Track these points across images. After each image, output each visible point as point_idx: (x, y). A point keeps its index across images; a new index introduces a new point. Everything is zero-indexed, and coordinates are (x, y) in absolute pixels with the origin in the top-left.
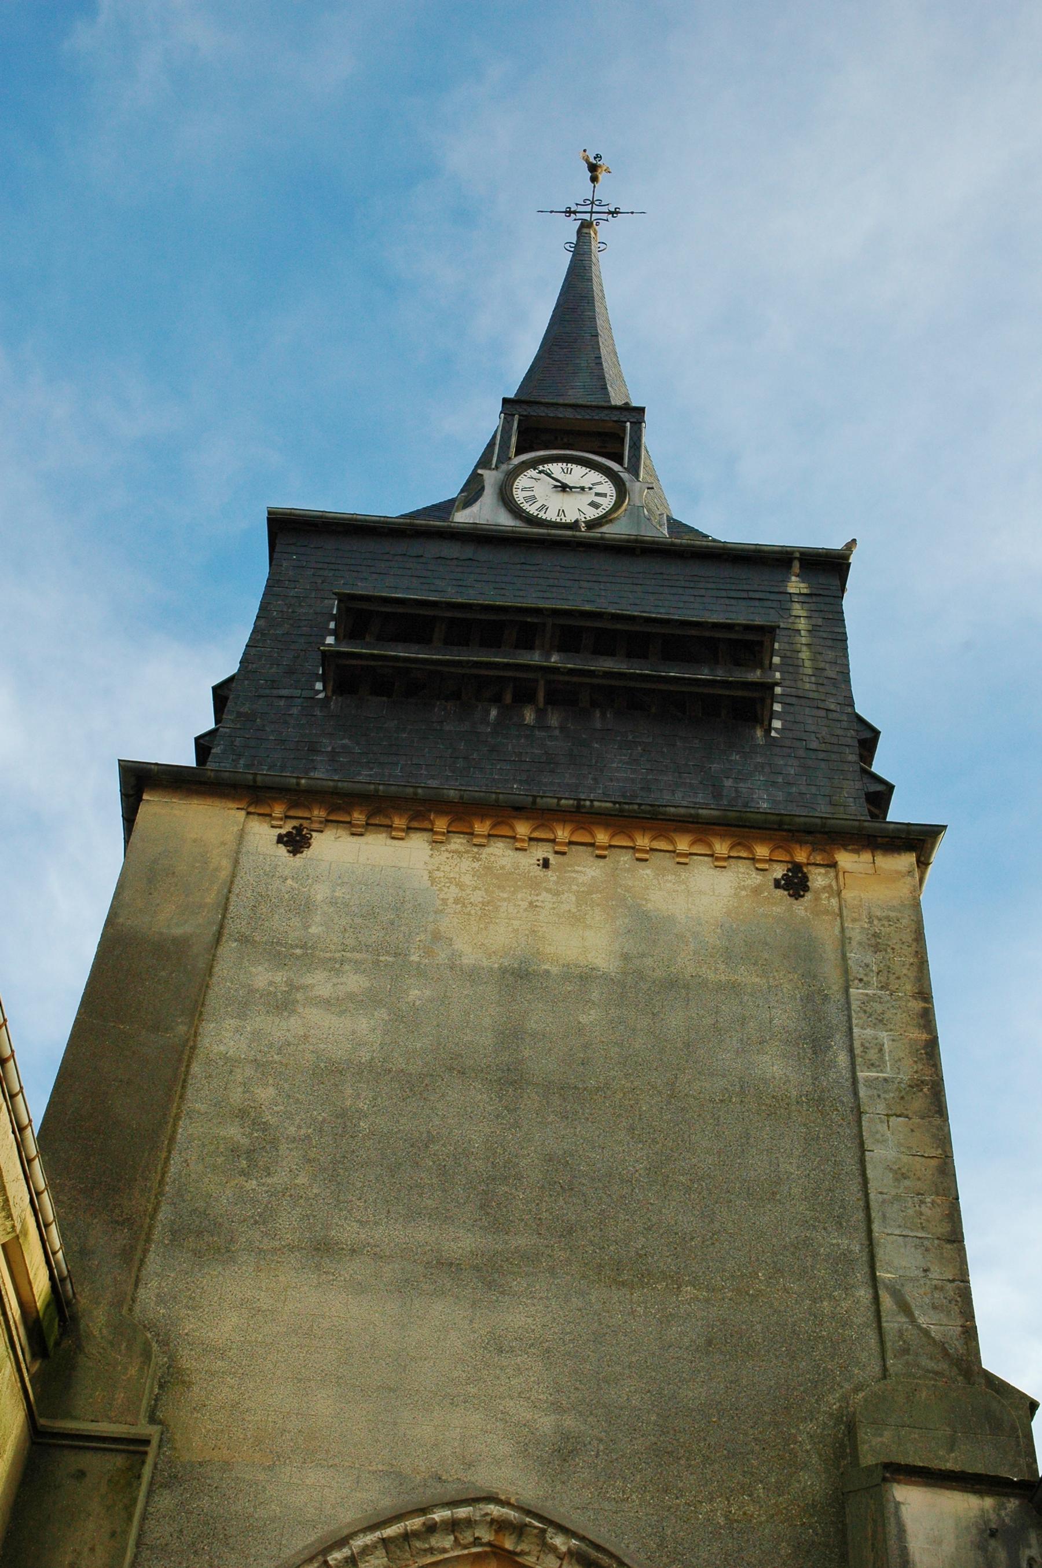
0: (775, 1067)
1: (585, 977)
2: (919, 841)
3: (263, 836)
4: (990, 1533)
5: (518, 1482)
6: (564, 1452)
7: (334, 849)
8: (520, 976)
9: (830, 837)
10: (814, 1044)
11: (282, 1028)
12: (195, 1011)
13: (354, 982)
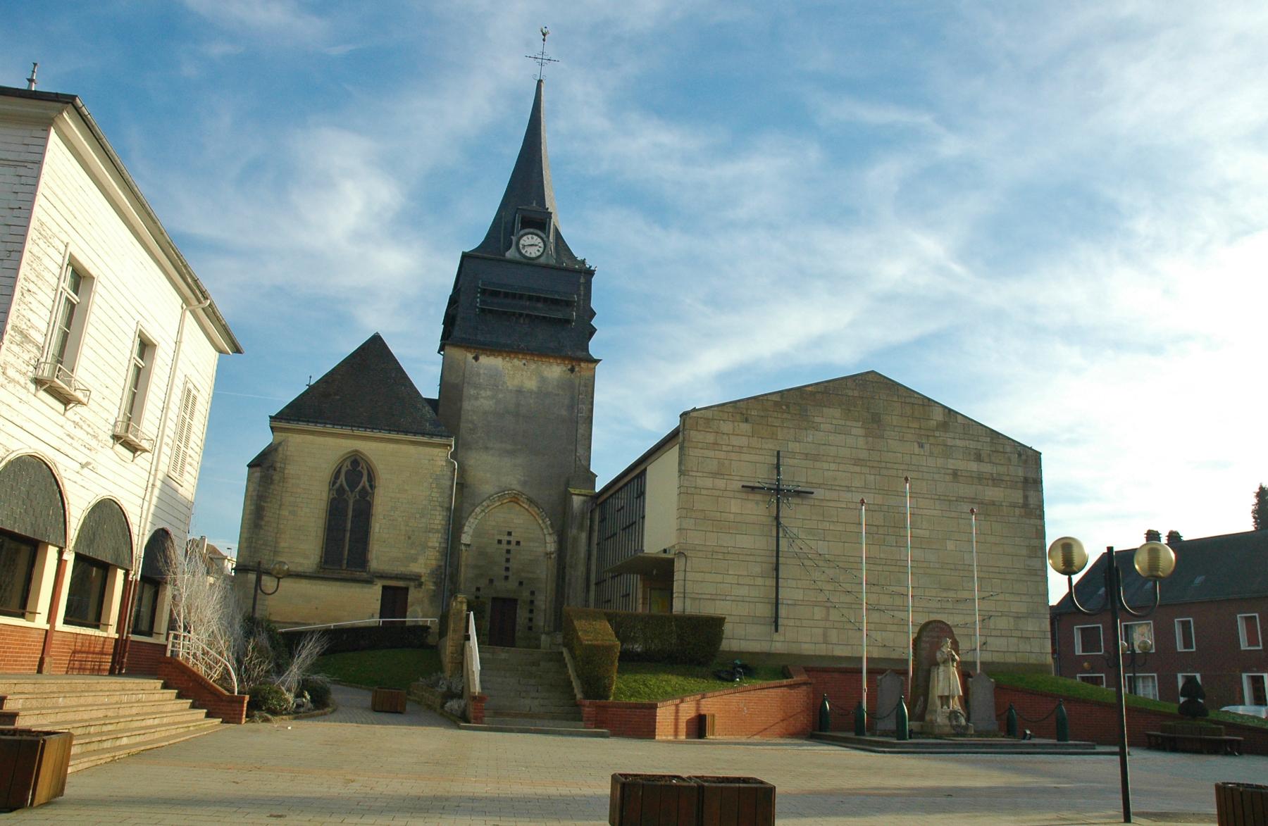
0: (564, 413)
1: (531, 392)
2: (1152, 536)
3: (470, 356)
4: (585, 502)
5: (519, 488)
6: (525, 483)
7: (484, 360)
8: (519, 391)
9: (580, 360)
10: (571, 407)
11: (477, 403)
12: (461, 401)
13: (489, 393)
